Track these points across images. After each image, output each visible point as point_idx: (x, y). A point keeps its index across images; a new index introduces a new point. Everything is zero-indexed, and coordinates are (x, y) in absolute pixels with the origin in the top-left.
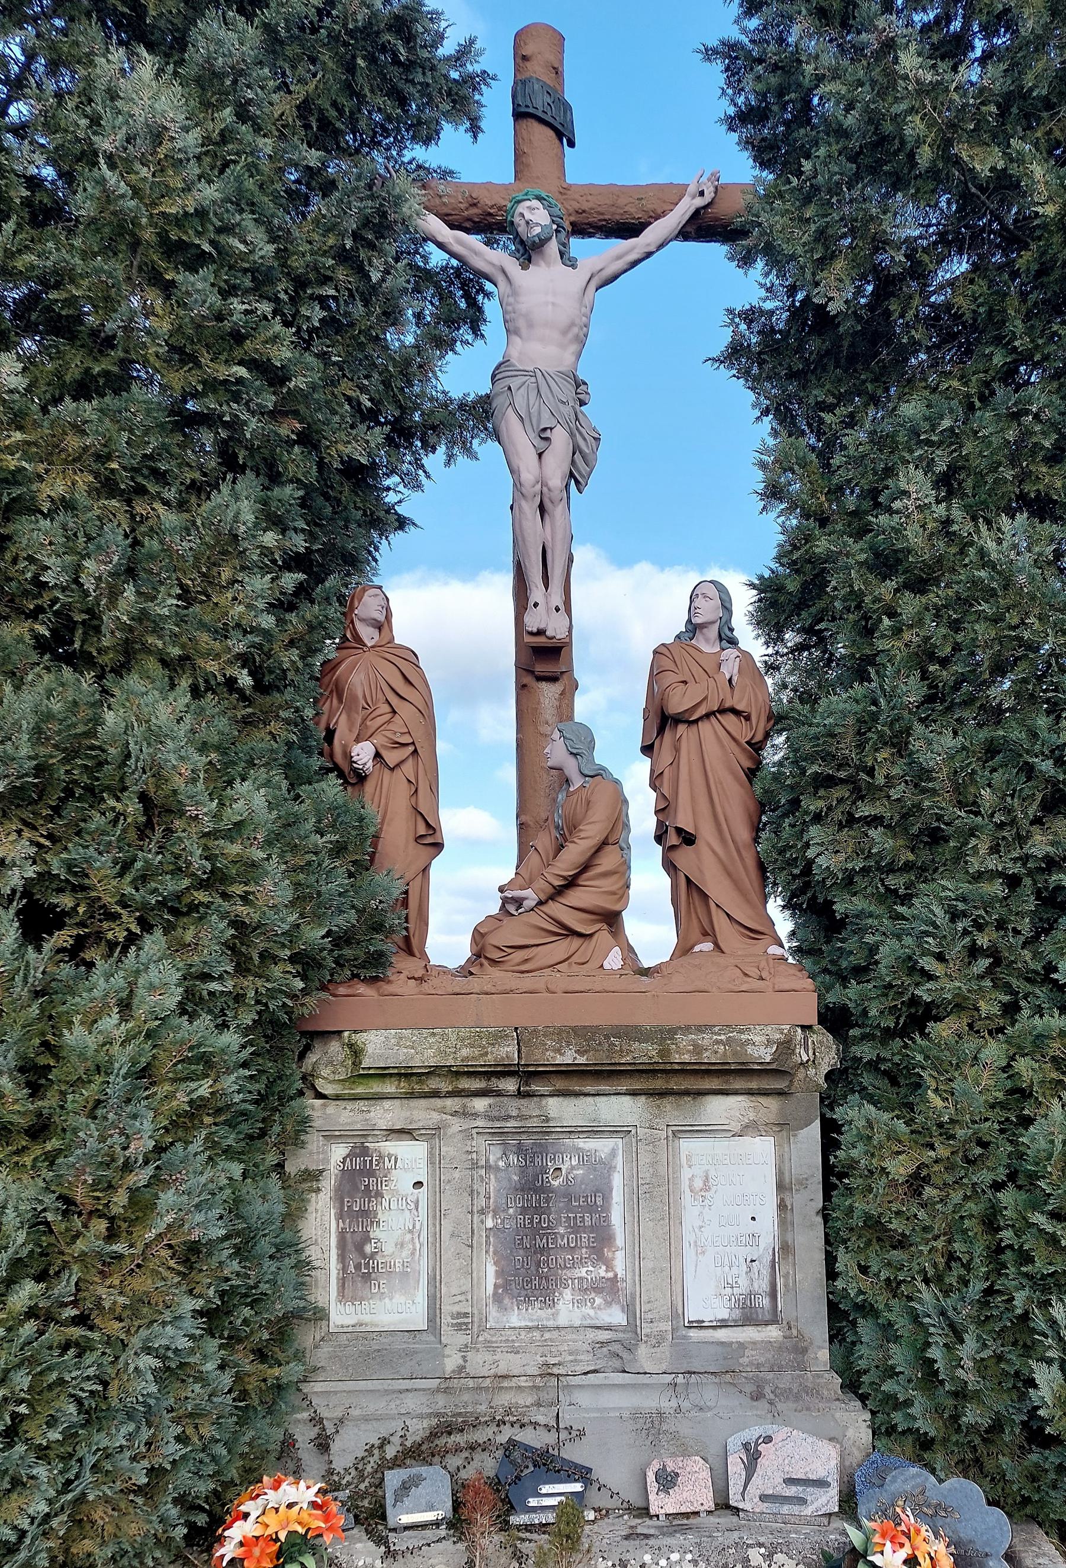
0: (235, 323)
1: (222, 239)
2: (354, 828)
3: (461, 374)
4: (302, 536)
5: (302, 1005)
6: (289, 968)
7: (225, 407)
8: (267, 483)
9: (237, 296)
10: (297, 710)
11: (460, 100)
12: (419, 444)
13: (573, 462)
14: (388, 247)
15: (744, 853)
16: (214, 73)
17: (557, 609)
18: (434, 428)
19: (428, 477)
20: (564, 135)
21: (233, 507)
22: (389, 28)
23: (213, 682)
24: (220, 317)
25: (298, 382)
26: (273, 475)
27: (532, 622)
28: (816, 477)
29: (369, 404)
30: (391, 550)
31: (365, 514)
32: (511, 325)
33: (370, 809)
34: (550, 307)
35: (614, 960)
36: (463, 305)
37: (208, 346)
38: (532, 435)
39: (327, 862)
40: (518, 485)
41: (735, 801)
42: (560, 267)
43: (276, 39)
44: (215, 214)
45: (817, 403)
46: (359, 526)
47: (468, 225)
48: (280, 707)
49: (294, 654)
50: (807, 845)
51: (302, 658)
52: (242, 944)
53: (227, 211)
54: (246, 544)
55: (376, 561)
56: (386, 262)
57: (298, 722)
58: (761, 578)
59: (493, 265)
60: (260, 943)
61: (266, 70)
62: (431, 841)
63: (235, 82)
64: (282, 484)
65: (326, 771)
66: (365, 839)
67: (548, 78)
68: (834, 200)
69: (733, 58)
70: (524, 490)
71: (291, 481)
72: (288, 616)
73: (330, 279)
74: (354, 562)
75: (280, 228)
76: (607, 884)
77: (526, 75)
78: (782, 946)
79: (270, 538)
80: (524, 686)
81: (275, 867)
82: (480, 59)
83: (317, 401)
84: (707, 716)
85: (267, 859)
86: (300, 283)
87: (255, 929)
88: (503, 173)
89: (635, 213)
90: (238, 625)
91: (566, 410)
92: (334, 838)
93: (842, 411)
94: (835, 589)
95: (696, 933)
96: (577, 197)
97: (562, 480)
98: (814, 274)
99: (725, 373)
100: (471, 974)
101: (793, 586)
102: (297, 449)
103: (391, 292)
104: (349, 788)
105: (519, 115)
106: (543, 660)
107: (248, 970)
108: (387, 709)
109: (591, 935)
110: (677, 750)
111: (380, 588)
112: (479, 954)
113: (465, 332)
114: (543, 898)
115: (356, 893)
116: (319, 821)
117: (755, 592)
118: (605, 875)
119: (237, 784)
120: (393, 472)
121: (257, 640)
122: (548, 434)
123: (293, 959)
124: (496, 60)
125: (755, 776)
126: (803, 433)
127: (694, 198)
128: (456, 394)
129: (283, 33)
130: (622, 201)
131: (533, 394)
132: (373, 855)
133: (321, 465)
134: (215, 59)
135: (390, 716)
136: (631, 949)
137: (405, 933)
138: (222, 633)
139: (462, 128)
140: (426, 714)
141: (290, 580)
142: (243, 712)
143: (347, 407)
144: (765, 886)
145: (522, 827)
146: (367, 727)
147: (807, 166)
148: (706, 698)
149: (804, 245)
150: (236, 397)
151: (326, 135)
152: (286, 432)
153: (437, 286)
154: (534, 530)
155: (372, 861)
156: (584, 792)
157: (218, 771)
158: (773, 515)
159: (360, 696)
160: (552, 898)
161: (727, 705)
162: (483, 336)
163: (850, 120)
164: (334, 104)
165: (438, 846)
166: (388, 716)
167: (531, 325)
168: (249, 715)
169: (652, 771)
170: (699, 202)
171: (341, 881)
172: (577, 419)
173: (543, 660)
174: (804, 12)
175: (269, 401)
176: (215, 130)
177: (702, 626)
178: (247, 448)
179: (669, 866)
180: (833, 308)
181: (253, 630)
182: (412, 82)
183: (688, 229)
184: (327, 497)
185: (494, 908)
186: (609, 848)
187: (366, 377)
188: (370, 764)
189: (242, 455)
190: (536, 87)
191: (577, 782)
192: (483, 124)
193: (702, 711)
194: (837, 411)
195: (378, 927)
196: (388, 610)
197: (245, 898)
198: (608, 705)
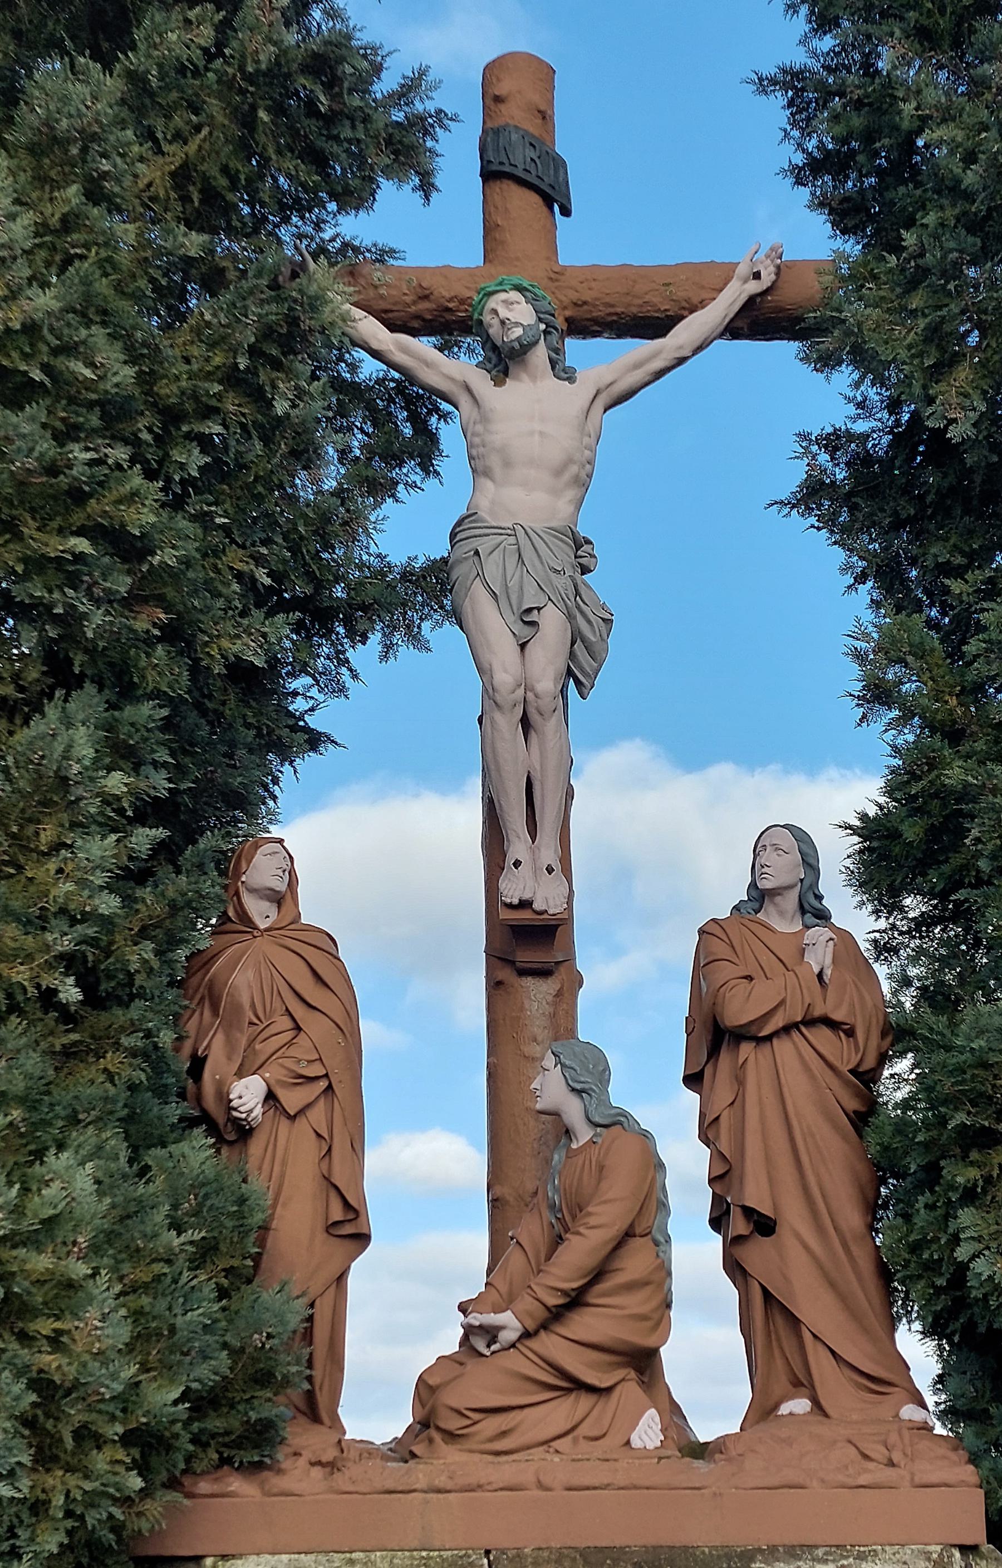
0: (75, 479)
1: (61, 363)
2: (230, 1215)
3: (405, 530)
4: (164, 774)
5: (139, 1514)
6: (121, 1455)
7: (56, 595)
8: (114, 699)
9: (77, 440)
10: (148, 1034)
11: (407, 150)
12: (341, 630)
13: (572, 655)
15: (854, 1249)
16: (55, 138)
17: (550, 870)
18: (365, 608)
19: (355, 676)
20: (554, 197)
21: (62, 739)
22: (306, 69)
23: (20, 998)
24: (52, 470)
25: (166, 557)
26: (122, 685)
27: (512, 889)
28: (941, 671)
29: (268, 581)
30: (294, 780)
31: (259, 735)
32: (479, 464)
33: (257, 1183)
34: (537, 437)
35: (648, 1432)
36: (408, 431)
37: (33, 511)
38: (511, 618)
39: (186, 1275)
40: (489, 693)
41: (836, 1165)
42: (551, 382)
43: (144, 90)
44: (51, 330)
45: (938, 565)
46: (251, 751)
47: (416, 324)
48: (122, 1029)
49: (147, 950)
50: (955, 1240)
51: (158, 953)
52: (48, 1415)
53: (69, 325)
54: (80, 791)
55: (274, 798)
56: (297, 387)
57: (152, 1056)
58: (864, 817)
59: (452, 380)
60: (76, 1414)
61: (129, 133)
62: (349, 1230)
63: (84, 150)
64: (138, 700)
65: (189, 1123)
66: (247, 1233)
68: (951, 286)
69: (799, 91)
70: (498, 698)
71: (150, 697)
72: (139, 893)
73: (217, 411)
74: (242, 803)
75: (145, 344)
76: (636, 1303)
77: (499, 122)
78: (923, 1405)
79: (116, 782)
80: (499, 984)
81: (104, 1289)
82: (434, 95)
83: (193, 582)
84: (787, 1029)
85: (93, 1276)
86: (171, 417)
87: (68, 1393)
90: (63, 911)
91: (562, 583)
92: (197, 1236)
93: (976, 576)
94: (978, 840)
95: (781, 1382)
98: (925, 387)
100: (414, 1455)
101: (912, 832)
102: (160, 650)
103: (303, 423)
104: (225, 1151)
105: (489, 175)
106: (527, 946)
107: (55, 1459)
108: (288, 1024)
109: (609, 1390)
110: (740, 1081)
111: (281, 841)
112: (425, 1423)
113: (411, 472)
114: (531, 1326)
115: (230, 1321)
116: (175, 1207)
117: (856, 839)
118: (630, 1287)
119: (50, 1158)
120: (304, 670)
121: (91, 931)
122: (534, 616)
123: (127, 1440)
125: (866, 1124)
126: (918, 607)
127: (745, 281)
128: (398, 558)
129: (154, 83)
131: (512, 561)
132: (257, 1258)
133: (196, 670)
134: (57, 121)
135: (291, 1034)
136: (675, 1409)
137: (306, 1386)
138: (40, 922)
139: (407, 188)
140: (348, 1031)
141: (144, 838)
142: (65, 1040)
143: (236, 587)
144: (891, 1305)
145: (495, 1203)
146: (255, 1052)
147: (910, 238)
148: (782, 1003)
149: (910, 347)
150: (73, 581)
151: (209, 212)
152: (146, 626)
154: (516, 756)
155: (256, 1267)
156: (595, 1151)
157: (22, 1135)
158: (879, 726)
160: (544, 1326)
161: (817, 1012)
163: (971, 178)
164: (225, 170)
165: (362, 1239)
167: (507, 464)
168: (75, 1044)
170: (754, 287)
171: (206, 1307)
172: (577, 593)
173: (527, 946)
174: (898, 33)
175: (122, 584)
176: (54, 214)
177: (773, 893)
178: (86, 651)
179: (735, 1268)
180: (954, 433)
181: (86, 918)
182: (336, 138)
183: (739, 324)
184: (203, 712)
185: (450, 1341)
186: (636, 1242)
187: (265, 543)
188: (258, 1111)
189: (78, 660)
190: (514, 137)
191: (584, 1134)
192: (438, 180)
193: (777, 1022)
194: (969, 576)
195: (264, 1378)
196: (292, 872)
197: (56, 1342)
198: (634, 1004)
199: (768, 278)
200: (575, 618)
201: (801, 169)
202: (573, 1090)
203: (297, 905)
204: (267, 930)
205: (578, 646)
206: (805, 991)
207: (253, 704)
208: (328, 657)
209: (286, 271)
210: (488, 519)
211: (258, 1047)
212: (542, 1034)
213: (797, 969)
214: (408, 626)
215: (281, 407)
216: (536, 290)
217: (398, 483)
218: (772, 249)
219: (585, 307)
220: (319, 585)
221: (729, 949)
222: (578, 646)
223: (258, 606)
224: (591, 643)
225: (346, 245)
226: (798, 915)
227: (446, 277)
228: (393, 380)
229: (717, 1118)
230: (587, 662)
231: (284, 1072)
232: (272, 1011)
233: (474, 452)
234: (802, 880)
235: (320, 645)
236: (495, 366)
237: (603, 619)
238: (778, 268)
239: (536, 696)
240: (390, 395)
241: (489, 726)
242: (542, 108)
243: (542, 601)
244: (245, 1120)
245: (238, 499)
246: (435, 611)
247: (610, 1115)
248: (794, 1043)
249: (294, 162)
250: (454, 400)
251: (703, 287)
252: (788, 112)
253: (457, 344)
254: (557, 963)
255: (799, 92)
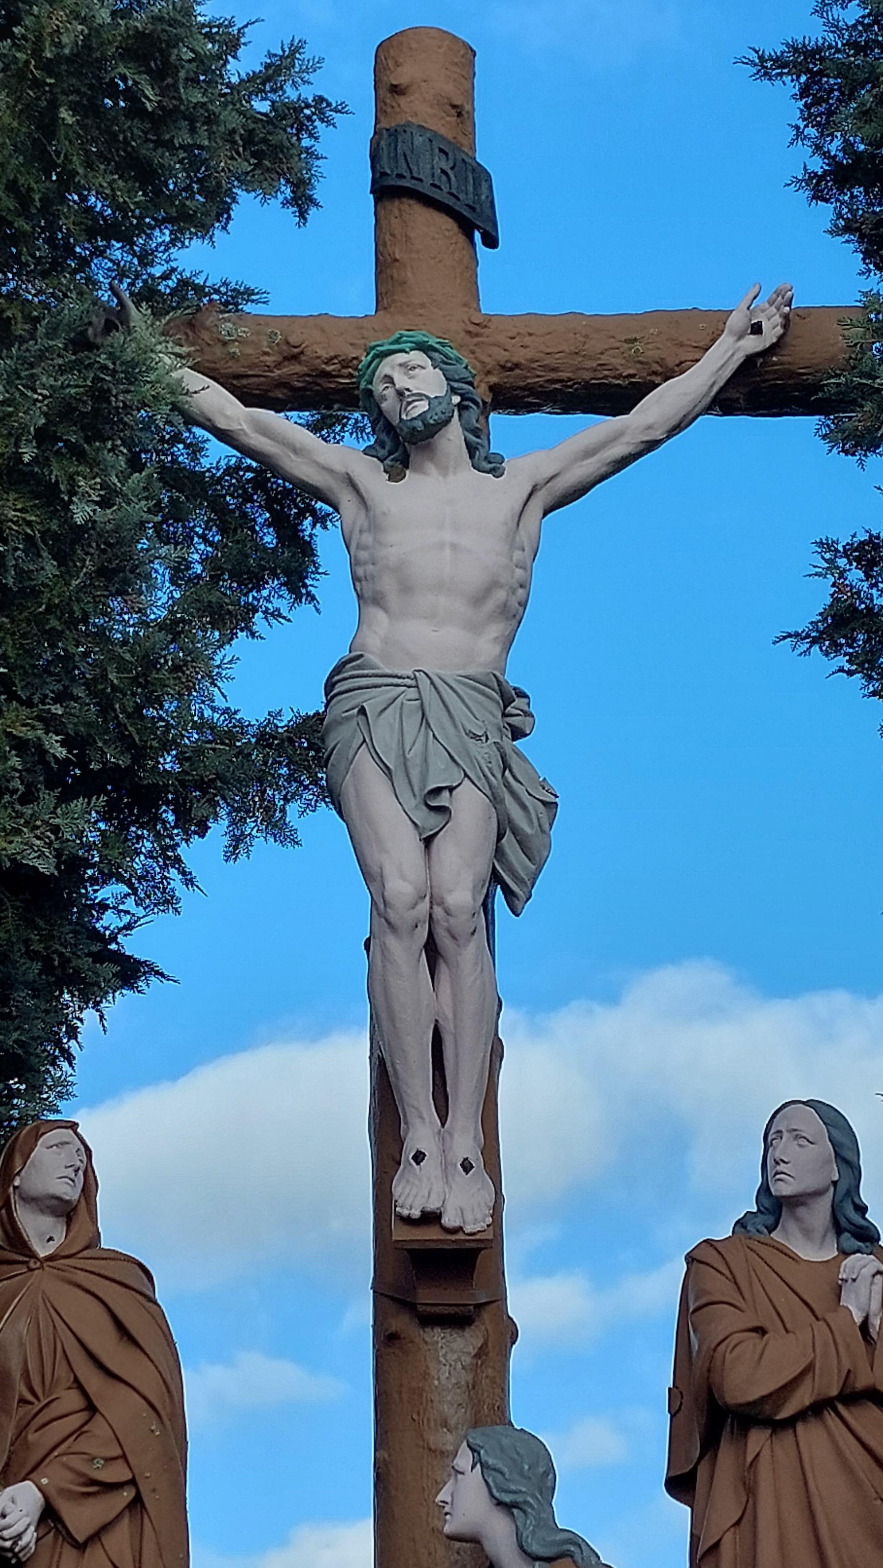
3: (265, 674)
11: (275, 152)
13: (499, 853)
14: (110, 457)
19: (189, 881)
20: (474, 220)
27: (414, 1194)
29: (61, 752)
30: (103, 1030)
34: (448, 551)
36: (270, 539)
38: (411, 803)
40: (380, 908)
42: (468, 476)
47: (279, 394)
55: (70, 1058)
59: (331, 471)
67: (442, 125)
70: (392, 915)
82: (311, 77)
84: (817, 1409)
88: (352, 295)
89: (623, 366)
91: (483, 752)
96: (502, 339)
97: (475, 890)
99: (821, 664)
105: (385, 191)
106: (435, 1282)
110: (750, 1489)
111: (73, 1126)
122: (443, 800)
124: (344, 79)
127: (740, 337)
128: (253, 714)
130: (596, 345)
131: (412, 723)
135: (83, 1416)
139: (275, 203)
140: (166, 1411)
143: (15, 761)
146: (27, 1446)
148: (809, 1369)
153: (218, 507)
154: (417, 996)
159: (17, 1374)
161: (862, 1382)
162: (312, 598)
166: (74, 1421)
167: (406, 588)
169: (695, 1540)
170: (752, 344)
172: (506, 766)
173: (435, 1282)
177: (795, 1201)
182: (169, 145)
188: (30, 1537)
190: (419, 140)
192: (318, 194)
193: (802, 1398)
196: (89, 1173)
199: (771, 332)
200: (502, 801)
201: (821, 178)
202: (499, 1503)
203: (94, 1220)
204: (50, 1258)
205: (508, 841)
206: (842, 1349)
207: (41, 923)
208: (150, 855)
209: (99, 321)
210: (381, 665)
211: (32, 1437)
212: (456, 1416)
213: (829, 1317)
214: (267, 810)
215: (80, 513)
216: (447, 350)
217: (255, 611)
218: (778, 293)
219: (518, 371)
220: (140, 753)
221: (730, 1285)
222: (508, 841)
223: (50, 787)
224: (527, 836)
225: (184, 283)
226: (831, 1238)
227: (323, 330)
228: (249, 468)
229: (716, 1546)
230: (521, 863)
231: (70, 1476)
232: (54, 1383)
233: (360, 572)
234: (835, 1183)
235: (140, 838)
236: (390, 453)
237: (544, 803)
238: (786, 317)
239: (448, 912)
240: (245, 491)
241: (378, 955)
242: (457, 102)
243: (455, 777)
244: (11, 1549)
245: (24, 636)
246: (306, 787)
247: (554, 1543)
248: (826, 1427)
249: (109, 178)
250: (332, 497)
251: (681, 345)
252: (801, 104)
253: (339, 420)
254: (479, 1307)
255: (815, 77)
